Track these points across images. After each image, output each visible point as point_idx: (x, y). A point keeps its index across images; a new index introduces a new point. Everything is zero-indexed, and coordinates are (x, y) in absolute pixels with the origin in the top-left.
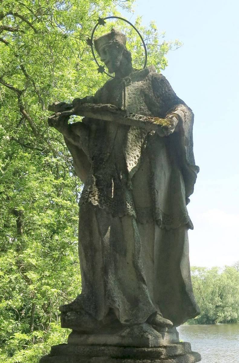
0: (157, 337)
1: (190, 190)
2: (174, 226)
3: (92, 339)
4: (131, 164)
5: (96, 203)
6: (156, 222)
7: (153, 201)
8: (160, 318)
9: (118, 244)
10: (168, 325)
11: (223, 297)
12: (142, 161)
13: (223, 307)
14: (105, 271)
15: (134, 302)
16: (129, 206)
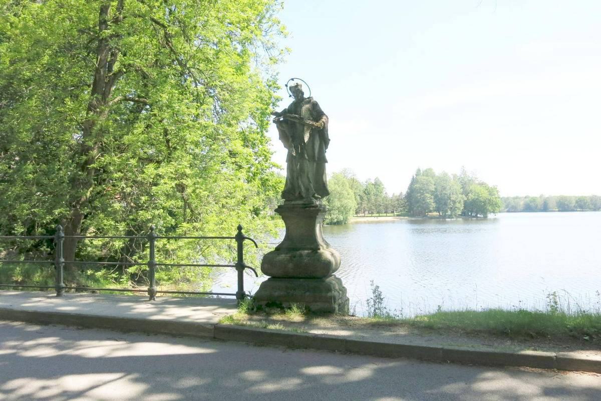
0: (316, 202)
1: (326, 147)
2: (320, 161)
3: (293, 203)
4: (306, 139)
5: (294, 155)
6: (314, 161)
7: (314, 153)
8: (316, 195)
9: (302, 170)
10: (319, 198)
11: (331, 201)
12: (310, 138)
13: (330, 211)
14: (298, 179)
15: (307, 190)
16: (306, 156)
